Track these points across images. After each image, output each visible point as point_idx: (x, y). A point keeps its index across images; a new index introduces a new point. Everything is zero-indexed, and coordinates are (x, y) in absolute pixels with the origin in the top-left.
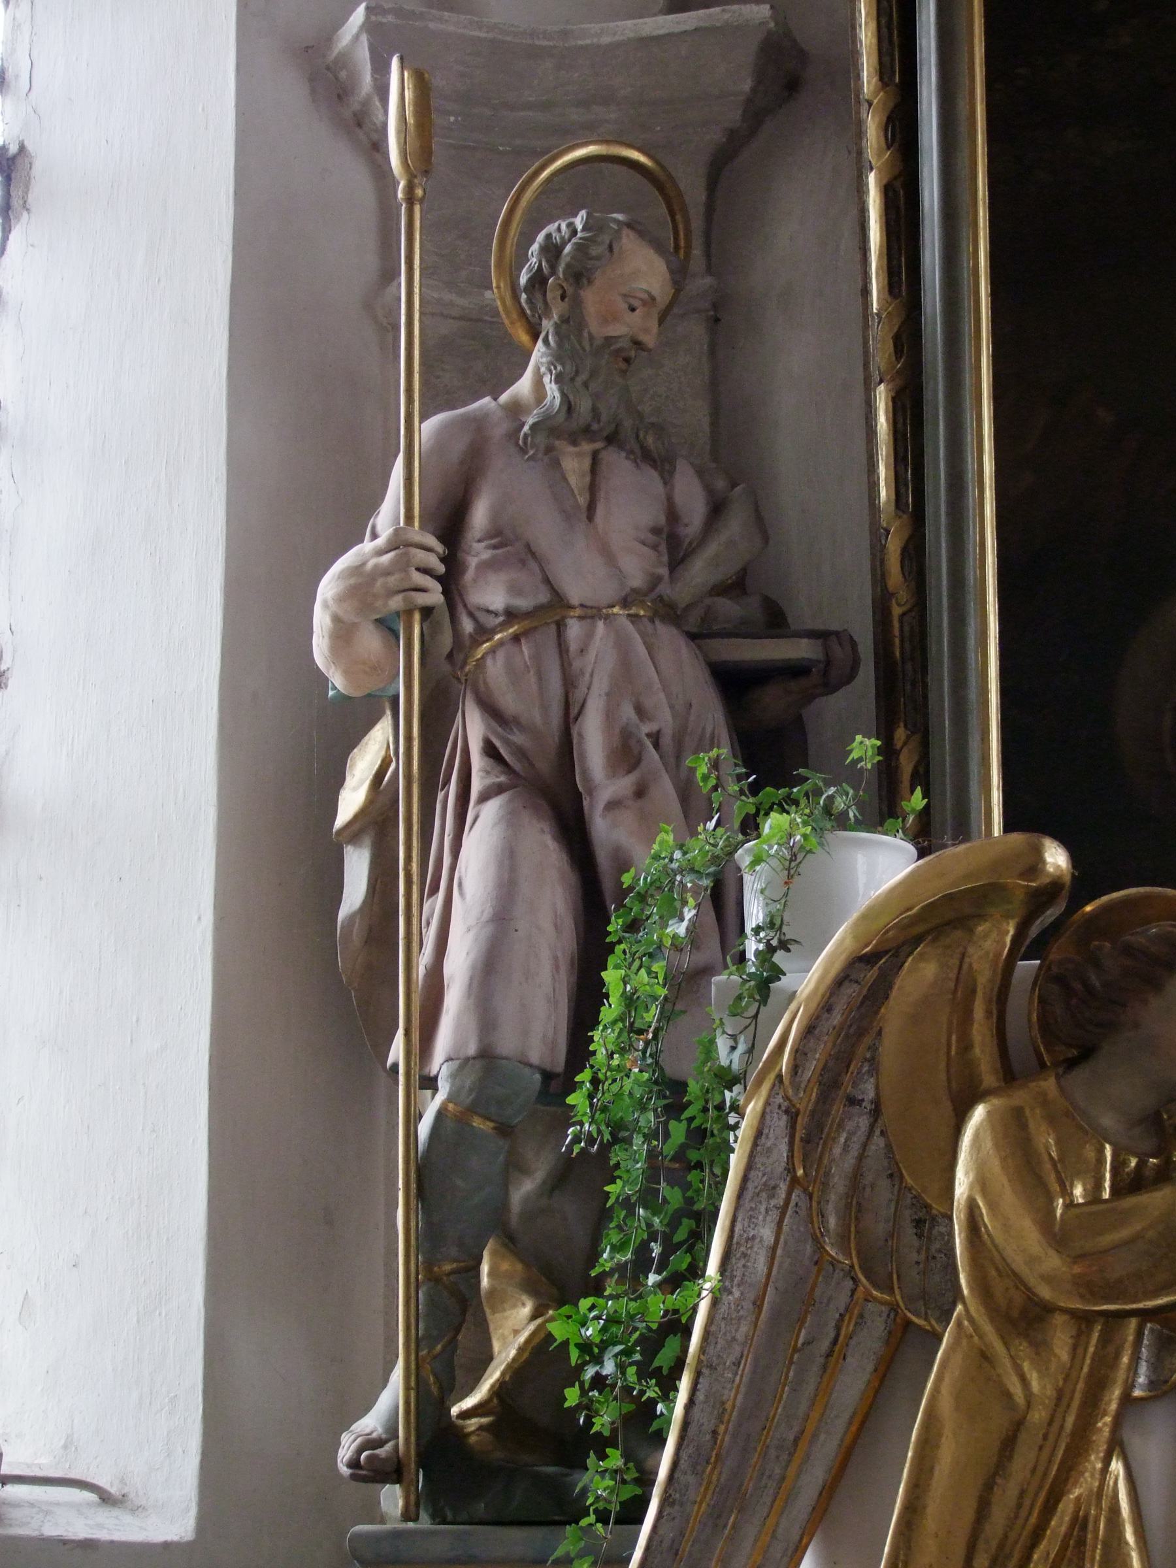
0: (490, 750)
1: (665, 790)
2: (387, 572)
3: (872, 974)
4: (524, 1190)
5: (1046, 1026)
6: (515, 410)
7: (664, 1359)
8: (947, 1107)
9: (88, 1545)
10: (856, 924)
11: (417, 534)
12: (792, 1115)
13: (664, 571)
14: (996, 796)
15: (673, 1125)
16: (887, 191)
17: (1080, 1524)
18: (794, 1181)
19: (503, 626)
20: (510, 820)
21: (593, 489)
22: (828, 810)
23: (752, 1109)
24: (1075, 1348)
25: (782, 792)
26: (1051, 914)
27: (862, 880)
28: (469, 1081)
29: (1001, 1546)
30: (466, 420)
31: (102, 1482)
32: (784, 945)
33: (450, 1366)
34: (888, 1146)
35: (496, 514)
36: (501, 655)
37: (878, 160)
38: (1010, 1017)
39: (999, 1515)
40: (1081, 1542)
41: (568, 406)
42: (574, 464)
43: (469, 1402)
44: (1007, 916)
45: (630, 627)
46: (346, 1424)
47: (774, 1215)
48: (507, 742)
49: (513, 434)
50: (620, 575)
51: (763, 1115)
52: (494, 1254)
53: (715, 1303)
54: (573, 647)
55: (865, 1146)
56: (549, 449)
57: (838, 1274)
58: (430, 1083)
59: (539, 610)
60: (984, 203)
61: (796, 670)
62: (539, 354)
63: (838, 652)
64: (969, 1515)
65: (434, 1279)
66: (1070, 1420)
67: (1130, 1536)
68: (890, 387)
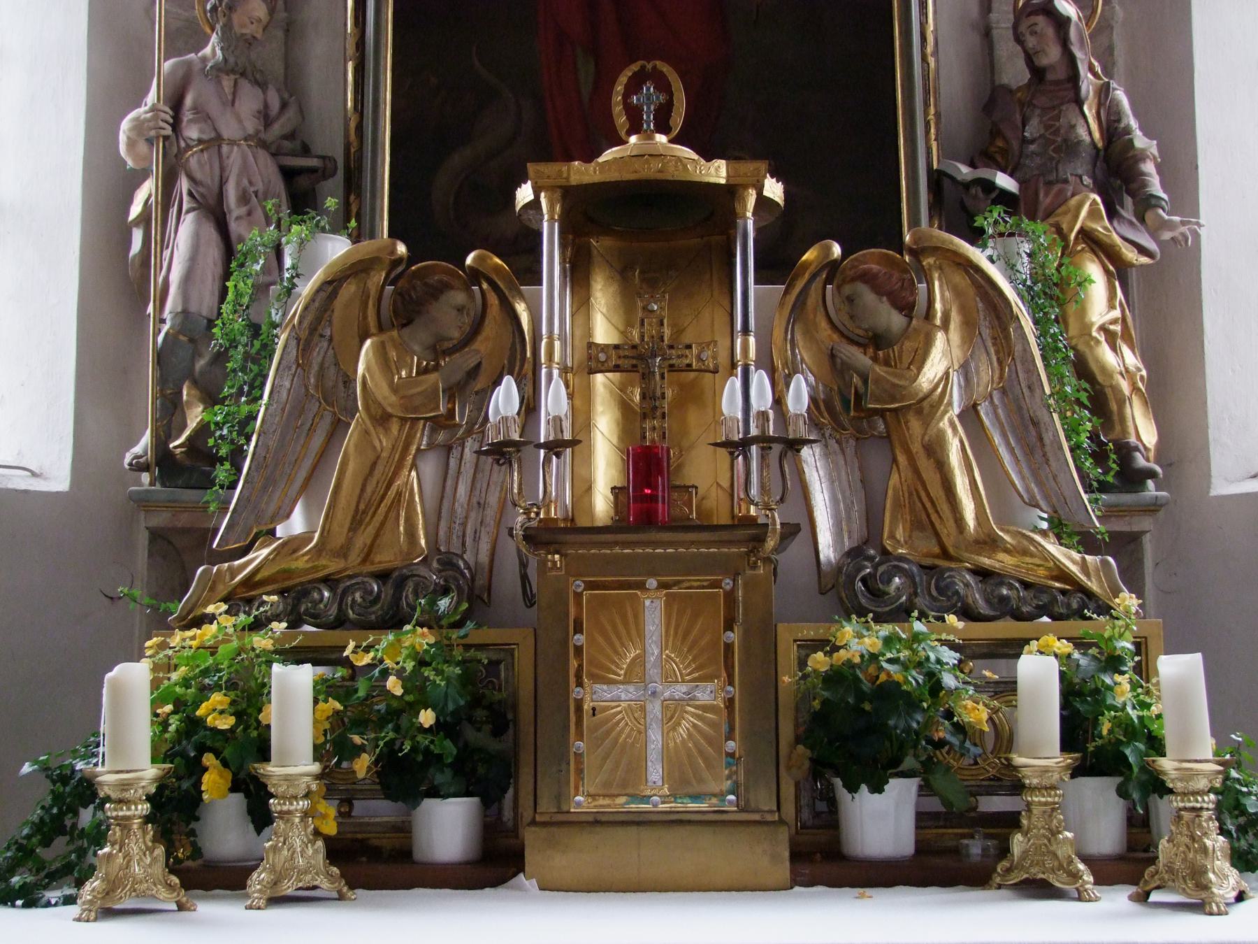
0: (190, 194)
1: (259, 213)
2: (149, 120)
3: (330, 289)
4: (201, 364)
5: (396, 312)
6: (204, 60)
7: (248, 429)
8: (357, 339)
9: (26, 492)
10: (325, 270)
11: (161, 106)
12: (298, 340)
13: (262, 128)
14: (386, 223)
15: (255, 341)
17: (399, 494)
18: (298, 365)
20: (198, 222)
21: (234, 94)
22: (317, 225)
23: (283, 337)
24: (400, 430)
25: (300, 217)
26: (400, 269)
27: (330, 252)
28: (178, 321)
29: (369, 501)
32: (298, 276)
33: (169, 428)
34: (335, 354)
35: (195, 102)
36: (195, 157)
38: (382, 307)
39: (369, 490)
40: (399, 501)
41: (225, 60)
42: (227, 83)
43: (177, 443)
44: (382, 270)
45: (246, 148)
46: (128, 450)
48: (197, 191)
50: (244, 129)
51: (287, 339)
52: (189, 388)
53: (267, 409)
54: (225, 155)
55: (326, 353)
56: (217, 77)
57: (313, 401)
58: (163, 321)
61: (312, 170)
62: (214, 38)
63: (329, 165)
64: (358, 491)
65: (163, 395)
66: (397, 456)
67: (417, 499)
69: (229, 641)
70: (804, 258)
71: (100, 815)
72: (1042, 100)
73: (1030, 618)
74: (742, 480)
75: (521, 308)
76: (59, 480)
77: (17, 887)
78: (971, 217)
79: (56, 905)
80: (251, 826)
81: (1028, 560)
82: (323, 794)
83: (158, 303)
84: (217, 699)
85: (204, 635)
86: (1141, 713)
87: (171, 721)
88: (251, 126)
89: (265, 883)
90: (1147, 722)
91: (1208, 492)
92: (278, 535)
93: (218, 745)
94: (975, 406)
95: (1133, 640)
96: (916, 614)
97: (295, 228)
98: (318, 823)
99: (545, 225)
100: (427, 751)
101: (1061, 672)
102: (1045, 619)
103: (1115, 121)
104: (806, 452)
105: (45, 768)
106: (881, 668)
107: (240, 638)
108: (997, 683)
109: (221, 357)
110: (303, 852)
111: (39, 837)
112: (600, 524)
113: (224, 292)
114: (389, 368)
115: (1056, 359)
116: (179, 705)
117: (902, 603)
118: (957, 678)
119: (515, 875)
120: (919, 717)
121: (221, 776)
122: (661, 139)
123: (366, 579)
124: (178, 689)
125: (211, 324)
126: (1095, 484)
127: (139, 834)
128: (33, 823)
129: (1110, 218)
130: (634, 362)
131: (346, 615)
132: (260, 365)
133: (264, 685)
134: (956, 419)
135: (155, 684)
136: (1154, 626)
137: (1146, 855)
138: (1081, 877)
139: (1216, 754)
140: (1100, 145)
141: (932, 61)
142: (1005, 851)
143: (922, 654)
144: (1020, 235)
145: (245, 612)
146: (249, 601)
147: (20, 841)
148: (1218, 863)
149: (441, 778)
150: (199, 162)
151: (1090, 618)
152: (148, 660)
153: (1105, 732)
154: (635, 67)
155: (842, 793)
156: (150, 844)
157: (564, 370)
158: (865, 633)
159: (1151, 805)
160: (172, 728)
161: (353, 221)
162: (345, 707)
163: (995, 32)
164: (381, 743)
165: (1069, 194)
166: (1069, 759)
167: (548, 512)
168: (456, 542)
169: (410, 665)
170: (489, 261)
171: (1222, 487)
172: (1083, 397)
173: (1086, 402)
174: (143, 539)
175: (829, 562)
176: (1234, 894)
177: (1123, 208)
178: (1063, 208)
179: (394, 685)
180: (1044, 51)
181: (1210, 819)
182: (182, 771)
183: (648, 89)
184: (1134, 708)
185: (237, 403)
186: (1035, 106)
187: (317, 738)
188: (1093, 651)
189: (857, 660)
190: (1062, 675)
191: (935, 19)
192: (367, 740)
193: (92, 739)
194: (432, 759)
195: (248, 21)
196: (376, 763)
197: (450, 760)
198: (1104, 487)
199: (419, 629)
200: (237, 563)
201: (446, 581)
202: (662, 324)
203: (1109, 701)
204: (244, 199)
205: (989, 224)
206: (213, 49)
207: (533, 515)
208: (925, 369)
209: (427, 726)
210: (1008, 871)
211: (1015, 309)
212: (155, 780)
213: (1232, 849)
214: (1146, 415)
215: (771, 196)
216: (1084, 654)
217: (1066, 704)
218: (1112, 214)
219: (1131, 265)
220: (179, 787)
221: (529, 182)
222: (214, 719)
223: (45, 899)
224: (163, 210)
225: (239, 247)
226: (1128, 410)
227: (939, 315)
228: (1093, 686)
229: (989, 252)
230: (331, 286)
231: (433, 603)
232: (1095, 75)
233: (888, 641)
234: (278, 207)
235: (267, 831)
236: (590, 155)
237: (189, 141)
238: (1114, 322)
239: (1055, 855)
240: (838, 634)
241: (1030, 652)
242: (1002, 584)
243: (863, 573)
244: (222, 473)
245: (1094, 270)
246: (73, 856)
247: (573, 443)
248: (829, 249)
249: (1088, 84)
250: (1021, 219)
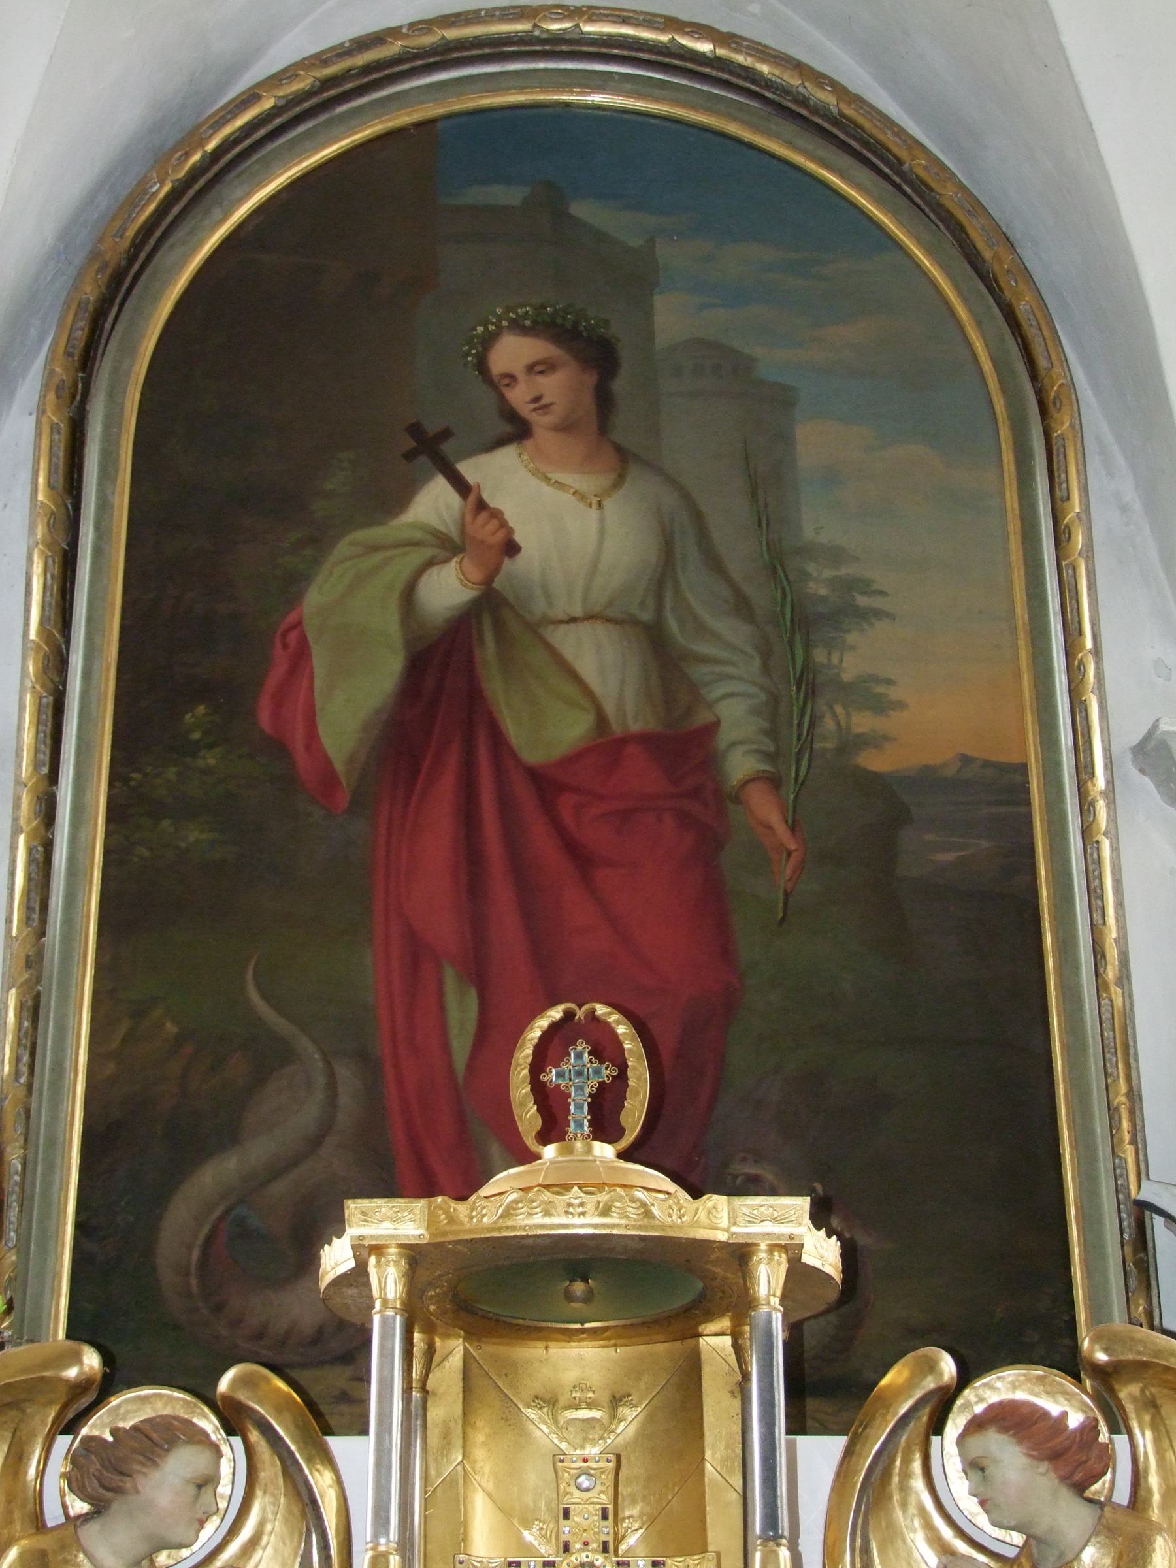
14: (64, 1302)
37: (28, 826)
44: (50, 1403)
60: (99, 867)
68: (19, 991)
70: (885, 1381)
75: (321, 1481)
122: (605, 1151)
154: (556, 1013)
183: (579, 1056)
248: (932, 1367)
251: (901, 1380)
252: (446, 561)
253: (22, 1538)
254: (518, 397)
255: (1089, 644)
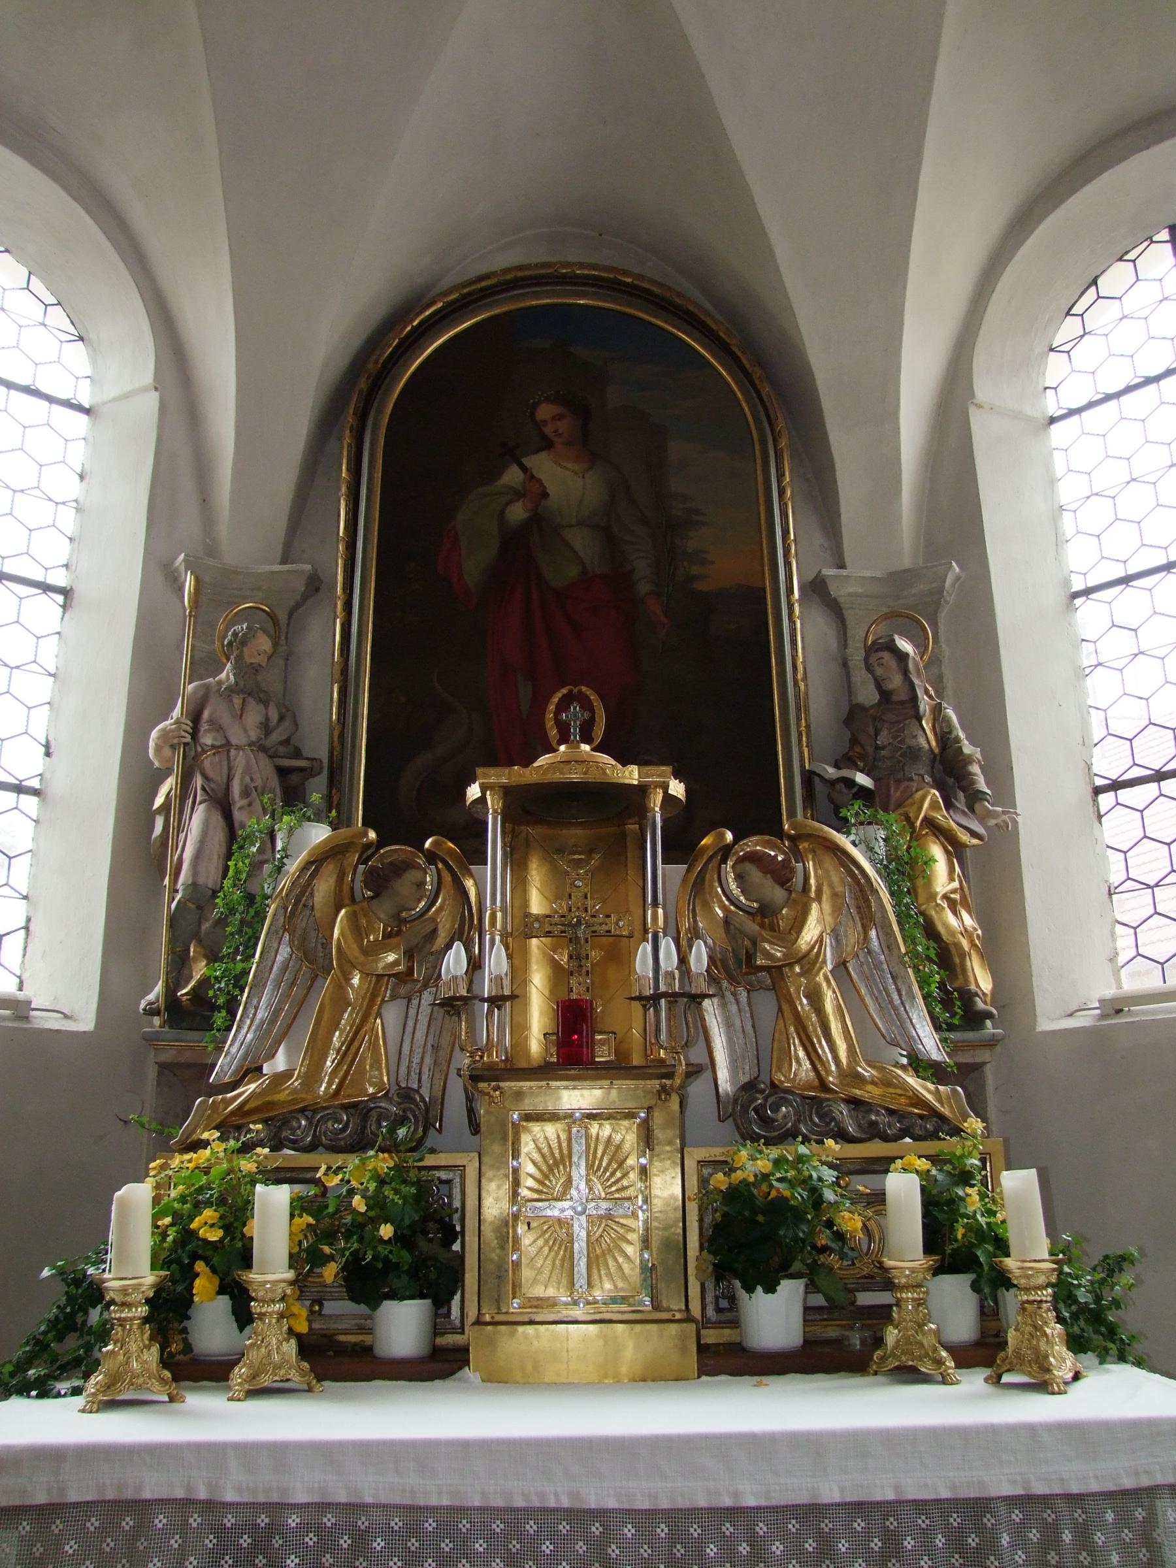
0: (203, 789)
1: (257, 806)
2: (173, 731)
6: (220, 683)
7: (242, 982)
11: (184, 720)
14: (360, 812)
16: (342, 625)
18: (285, 930)
19: (210, 750)
20: (208, 810)
21: (242, 710)
26: (370, 852)
27: (314, 837)
30: (205, 685)
31: (65, 1012)
32: (287, 857)
35: (211, 715)
36: (209, 759)
42: (237, 701)
43: (184, 991)
44: (356, 852)
46: (143, 997)
47: (278, 940)
48: (209, 787)
49: (218, 690)
50: (249, 737)
53: (257, 966)
54: (232, 758)
58: (177, 891)
59: (221, 746)
61: (302, 769)
65: (173, 952)
69: (220, 1164)
70: (702, 843)
71: (106, 1314)
72: (890, 717)
73: (896, 1138)
74: (653, 1028)
75: (469, 884)
76: (86, 1022)
77: (33, 1378)
78: (837, 809)
79: (65, 1395)
80: (235, 1325)
81: (891, 1090)
82: (297, 1297)
83: (173, 877)
84: (209, 1214)
85: (199, 1158)
86: (988, 1220)
87: (169, 1233)
88: (254, 734)
89: (244, 1377)
90: (994, 1227)
91: (1035, 1029)
92: (264, 1072)
93: (209, 1253)
94: (844, 963)
95: (979, 1156)
96: (800, 1139)
97: (286, 818)
98: (292, 1322)
99: (490, 817)
100: (386, 1260)
101: (922, 1186)
102: (908, 1140)
103: (947, 733)
104: (706, 1003)
105: (61, 1272)
106: (771, 1186)
107: (230, 1161)
108: (868, 1194)
109: (222, 922)
110: (278, 1348)
111: (54, 1333)
112: (535, 1064)
113: (226, 869)
114: (360, 934)
115: (909, 923)
116: (177, 1218)
117: (788, 1129)
118: (835, 1191)
119: (460, 1368)
120: (805, 1228)
121: (210, 1282)
122: (585, 748)
123: (336, 1110)
124: (176, 1205)
125: (214, 893)
126: (944, 1026)
127: (138, 1333)
128: (49, 1320)
129: (947, 810)
130: (563, 928)
131: (320, 1140)
132: (253, 929)
133: (248, 1202)
134: (829, 974)
135: (156, 1200)
136: (996, 1145)
137: (997, 1340)
138: (944, 1364)
139: (1052, 1254)
140: (937, 751)
141: (802, 687)
142: (879, 1342)
143: (806, 1173)
144: (877, 824)
145: (234, 1138)
146: (239, 1128)
147: (37, 1337)
148: (1057, 1348)
149: (397, 1283)
150: (211, 764)
151: (944, 1139)
152: (152, 1179)
153: (959, 1236)
154: (565, 691)
155: (742, 1294)
156: (147, 1342)
157: (505, 936)
158: (758, 1156)
159: (1000, 1299)
160: (170, 1239)
161: (334, 811)
162: (317, 1221)
163: (851, 664)
164: (347, 1253)
165: (914, 789)
166: (931, 1261)
167: (489, 1056)
168: (414, 1077)
169: (372, 1186)
170: (444, 846)
171: (1045, 1024)
172: (932, 953)
173: (935, 958)
174: (152, 1072)
175: (727, 1094)
176: (1071, 1375)
177: (956, 800)
178: (910, 801)
179: (358, 1203)
180: (889, 678)
181: (1049, 1310)
182: (178, 1276)
183: (575, 708)
184: (983, 1215)
185: (234, 959)
186: (884, 721)
187: (293, 1248)
188: (948, 1167)
189: (752, 1179)
190: (923, 1188)
191: (803, 653)
192: (335, 1250)
193: (102, 1247)
194: (390, 1266)
195: (256, 653)
196: (343, 1269)
197: (405, 1268)
198: (951, 1028)
199: (381, 1155)
200: (229, 1095)
201: (404, 1112)
202: (586, 897)
203: (962, 1210)
204: (246, 793)
205: (851, 815)
206: (227, 674)
207: (477, 1058)
208: (803, 934)
209: (386, 1238)
210: (883, 1358)
211: (875, 884)
212: (153, 1286)
213: (1068, 1334)
214: (982, 966)
215: (675, 794)
216: (940, 1170)
217: (926, 1214)
218: (949, 805)
219: (965, 846)
220: (175, 1290)
221: (477, 783)
222: (206, 1232)
223: (55, 1391)
224: (180, 800)
225: (240, 833)
226: (968, 963)
227: (813, 888)
228: (949, 1197)
229: (852, 837)
230: (316, 862)
231: (392, 1130)
232: (930, 697)
233: (778, 1163)
234: (273, 801)
235: (248, 1329)
236: (527, 762)
237: (205, 747)
238: (954, 891)
239: (921, 1345)
240: (736, 1158)
241: (896, 1170)
242: (870, 1111)
243: (756, 1104)
244: (219, 1018)
245: (936, 851)
246: (82, 1351)
247: (513, 997)
248: (723, 836)
249: (925, 704)
250: (876, 810)
251: (710, 842)
252: (517, 501)
253: (348, 905)
254: (548, 430)
255: (792, 537)
